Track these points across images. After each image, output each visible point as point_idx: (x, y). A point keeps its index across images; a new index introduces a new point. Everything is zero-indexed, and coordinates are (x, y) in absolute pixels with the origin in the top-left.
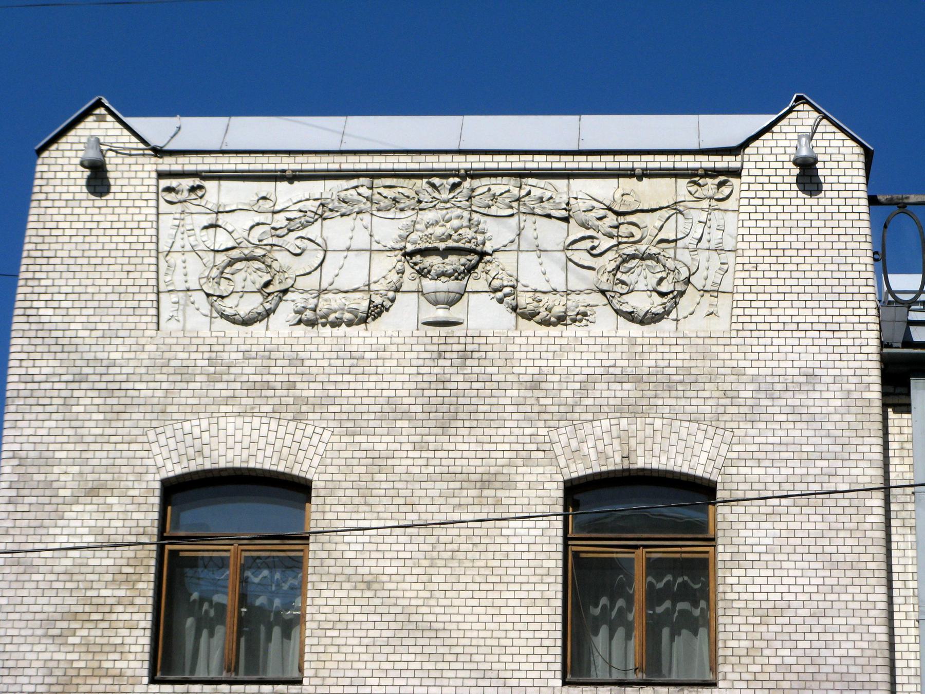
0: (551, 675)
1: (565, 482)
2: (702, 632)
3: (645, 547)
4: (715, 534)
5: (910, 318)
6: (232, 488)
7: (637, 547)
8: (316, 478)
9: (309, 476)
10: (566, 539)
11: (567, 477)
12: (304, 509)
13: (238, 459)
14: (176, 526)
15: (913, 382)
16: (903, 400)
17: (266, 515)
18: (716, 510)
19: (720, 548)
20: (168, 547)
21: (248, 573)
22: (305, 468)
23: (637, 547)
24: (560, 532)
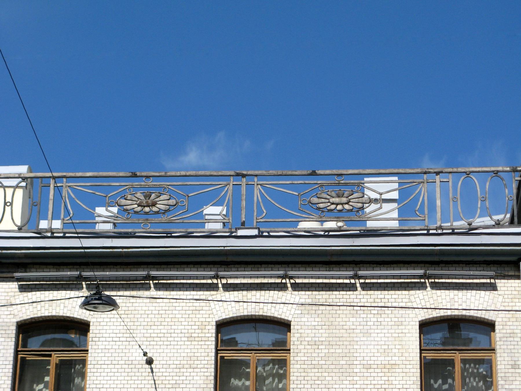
9: (89, 320)
10: (421, 350)
12: (286, 335)
19: (498, 355)
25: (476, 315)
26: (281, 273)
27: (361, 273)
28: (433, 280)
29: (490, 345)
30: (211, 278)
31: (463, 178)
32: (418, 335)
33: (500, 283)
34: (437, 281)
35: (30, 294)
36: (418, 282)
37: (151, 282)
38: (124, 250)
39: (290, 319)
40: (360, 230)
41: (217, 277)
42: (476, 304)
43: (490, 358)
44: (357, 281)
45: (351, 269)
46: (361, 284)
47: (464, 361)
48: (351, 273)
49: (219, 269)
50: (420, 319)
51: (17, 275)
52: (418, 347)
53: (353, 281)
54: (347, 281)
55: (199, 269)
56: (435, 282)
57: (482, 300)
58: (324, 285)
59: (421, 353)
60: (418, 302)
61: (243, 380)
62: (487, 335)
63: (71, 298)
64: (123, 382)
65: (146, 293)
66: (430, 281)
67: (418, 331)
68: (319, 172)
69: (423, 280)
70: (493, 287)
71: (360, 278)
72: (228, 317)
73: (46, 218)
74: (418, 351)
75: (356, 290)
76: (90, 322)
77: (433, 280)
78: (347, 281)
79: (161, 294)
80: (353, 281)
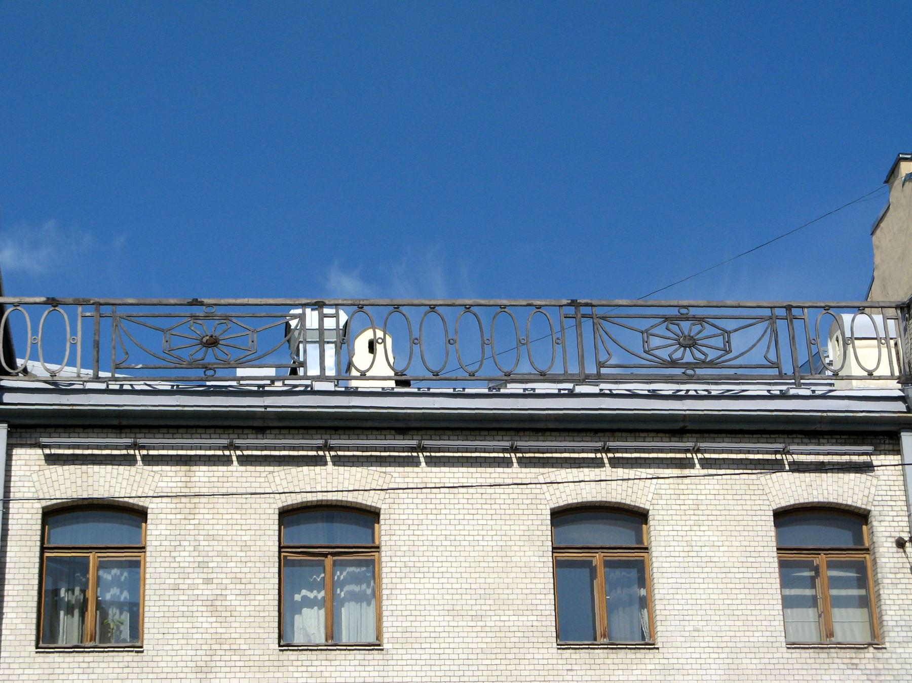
0: (152, 631)
1: (551, 509)
2: (373, 602)
3: (333, 554)
4: (380, 543)
5: (327, 346)
6: (108, 513)
7: (325, 555)
8: (651, 508)
9: (378, 506)
10: (280, 547)
11: (775, 508)
12: (140, 527)
13: (619, 496)
14: (49, 542)
15: (902, 434)
16: (896, 448)
17: (345, 533)
18: (380, 528)
19: (383, 554)
20: (283, 554)
21: (101, 573)
22: (778, 502)
23: (325, 555)
24: (38, 543)
25: (334, 498)
26: (129, 441)
27: (332, 442)
28: (428, 454)
29: (373, 541)
30: (127, 447)
31: (46, 313)
32: (277, 527)
33: (877, 460)
34: (433, 454)
35: (620, 470)
36: (408, 456)
37: (420, 454)
38: (825, 414)
39: (647, 507)
40: (649, 391)
41: (135, 446)
42: (335, 484)
43: (372, 558)
44: (513, 455)
45: (319, 436)
46: (610, 459)
47: (609, 564)
48: (129, 441)
49: (138, 435)
50: (280, 505)
51: (44, 440)
52: (277, 544)
53: (227, 453)
54: (220, 453)
55: (351, 437)
56: (431, 457)
57: (352, 479)
58: (713, 462)
59: (280, 552)
60: (296, 483)
61: (315, 592)
62: (366, 526)
63: (629, 479)
64: (428, 597)
65: (692, 472)
66: (425, 454)
67: (277, 522)
68: (206, 301)
69: (321, 453)
70: (866, 468)
71: (331, 449)
72: (364, 502)
73: (23, 358)
74: (277, 549)
75: (325, 464)
76: (380, 509)
77: (428, 454)
78: (220, 453)
79: (621, 472)
80: (227, 453)
